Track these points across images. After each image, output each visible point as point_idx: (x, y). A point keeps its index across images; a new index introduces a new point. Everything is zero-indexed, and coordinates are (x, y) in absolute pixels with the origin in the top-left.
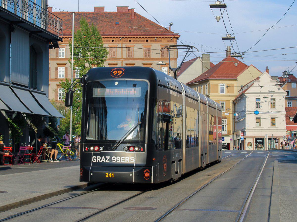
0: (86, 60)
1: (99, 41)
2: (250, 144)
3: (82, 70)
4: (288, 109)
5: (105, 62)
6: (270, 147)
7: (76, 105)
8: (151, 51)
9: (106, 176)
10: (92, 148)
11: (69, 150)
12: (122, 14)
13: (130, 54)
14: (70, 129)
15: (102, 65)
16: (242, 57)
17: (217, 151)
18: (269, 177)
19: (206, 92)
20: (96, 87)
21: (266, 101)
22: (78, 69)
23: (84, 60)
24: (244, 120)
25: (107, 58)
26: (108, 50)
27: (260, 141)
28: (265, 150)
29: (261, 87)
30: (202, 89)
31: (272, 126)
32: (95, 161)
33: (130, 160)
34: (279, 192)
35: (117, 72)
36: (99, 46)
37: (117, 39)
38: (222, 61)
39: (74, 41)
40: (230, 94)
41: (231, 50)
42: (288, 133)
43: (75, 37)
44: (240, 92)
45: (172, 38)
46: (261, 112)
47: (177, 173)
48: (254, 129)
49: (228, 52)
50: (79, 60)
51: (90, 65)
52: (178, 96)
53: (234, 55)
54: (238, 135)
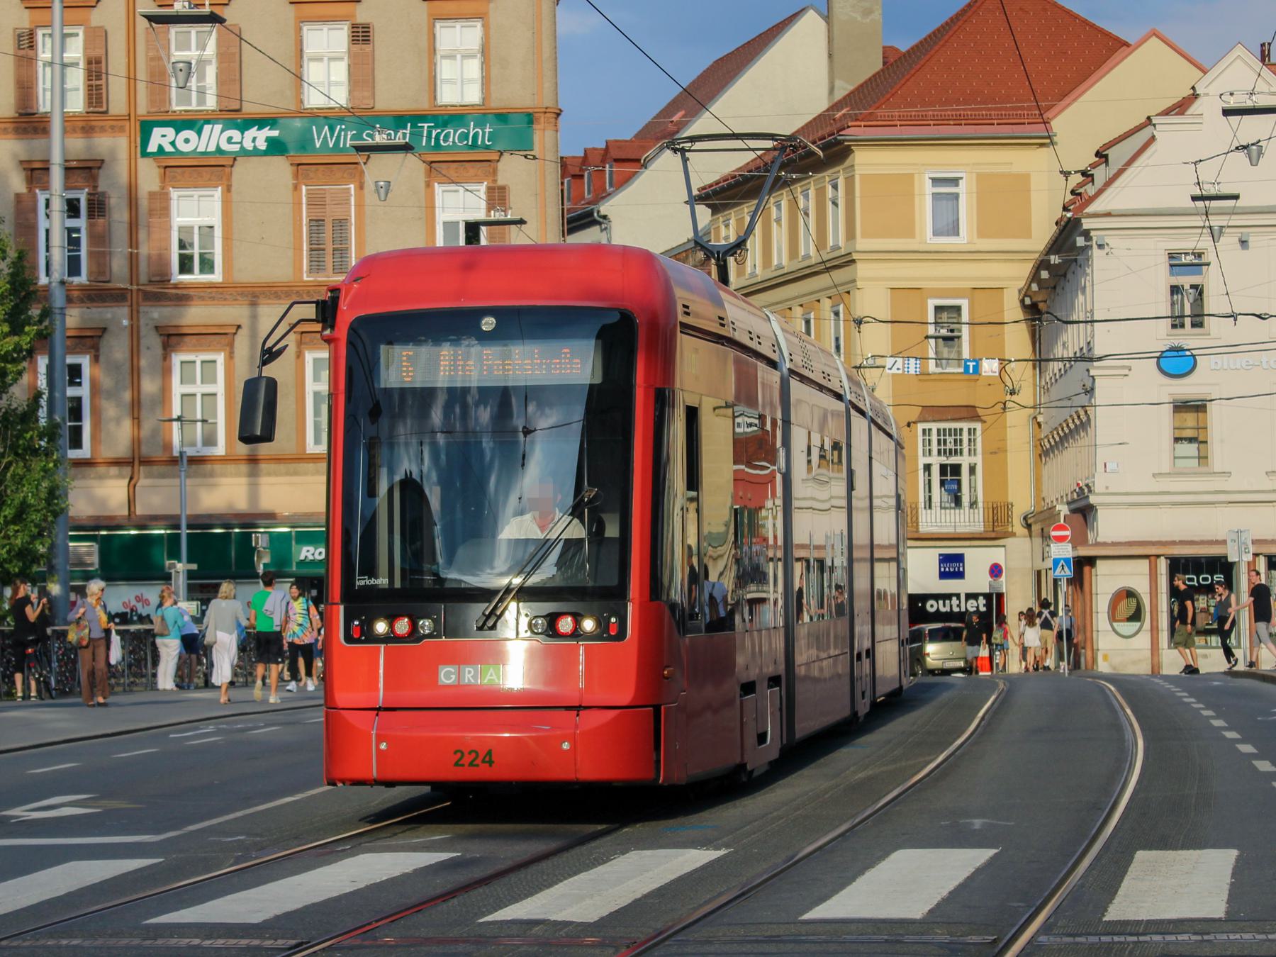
47: (762, 738)
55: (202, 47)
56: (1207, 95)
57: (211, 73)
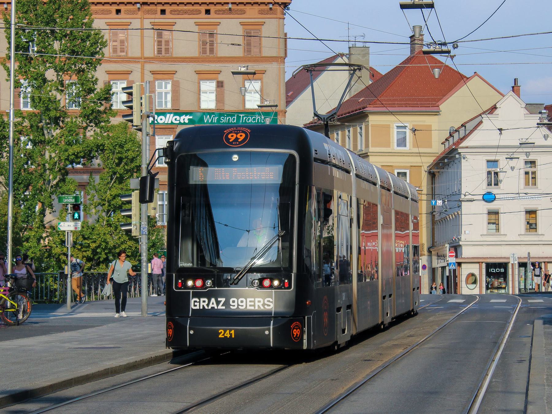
0: (47, 61)
1: (83, 13)
2: (472, 279)
3: (39, 88)
5: (98, 68)
6: (522, 286)
7: (22, 181)
8: (216, 39)
9: (220, 336)
10: (190, 283)
11: (5, 297)
13: (163, 47)
14: (7, 243)
15: (90, 76)
16: (452, 54)
17: (412, 290)
18: (521, 361)
19: (361, 146)
20: (192, 166)
21: (512, 168)
22: (27, 85)
23: (44, 62)
24: (458, 217)
25: (103, 56)
26: (107, 35)
27: (497, 270)
28: (511, 292)
29: (499, 132)
30: (349, 138)
32: (198, 307)
33: (264, 304)
34: (546, 401)
35: (235, 135)
36: (82, 24)
37: (130, 7)
38: (400, 64)
39: (17, 11)
40: (422, 150)
41: (423, 35)
43: (18, 3)
44: (447, 143)
45: (271, 6)
46: (501, 196)
47: (343, 331)
49: (416, 42)
50: (30, 63)
51: (58, 75)
52: (344, 179)
53: (432, 49)
54: (441, 256)
55: (166, 88)
56: (500, 108)
57: (169, 97)
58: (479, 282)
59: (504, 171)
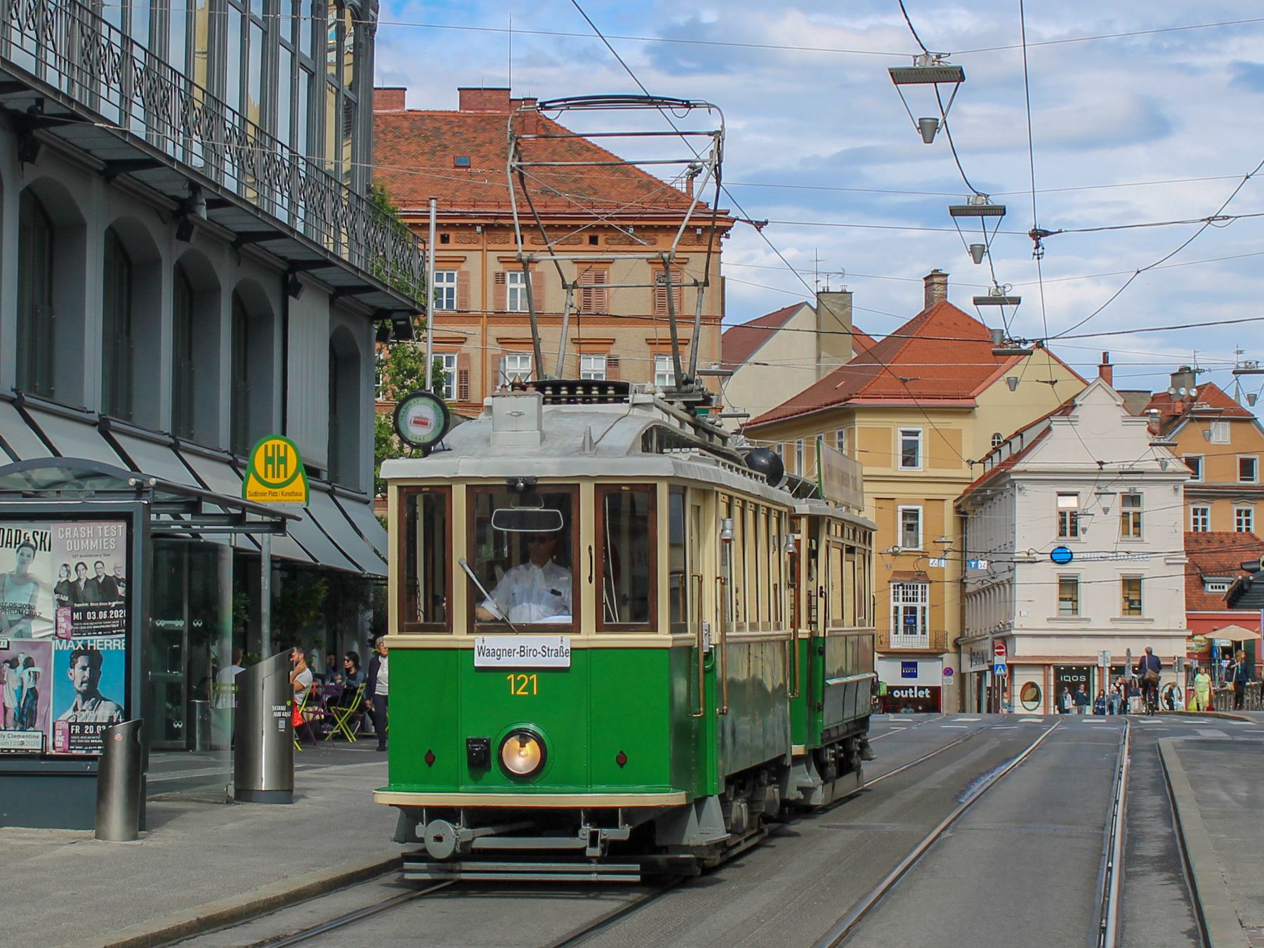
4: (1197, 541)
12: (482, 121)
31: (1124, 614)
42: (1193, 645)
48: (1049, 626)
56: (1081, 405)
58: (1042, 698)
59: (1089, 513)
